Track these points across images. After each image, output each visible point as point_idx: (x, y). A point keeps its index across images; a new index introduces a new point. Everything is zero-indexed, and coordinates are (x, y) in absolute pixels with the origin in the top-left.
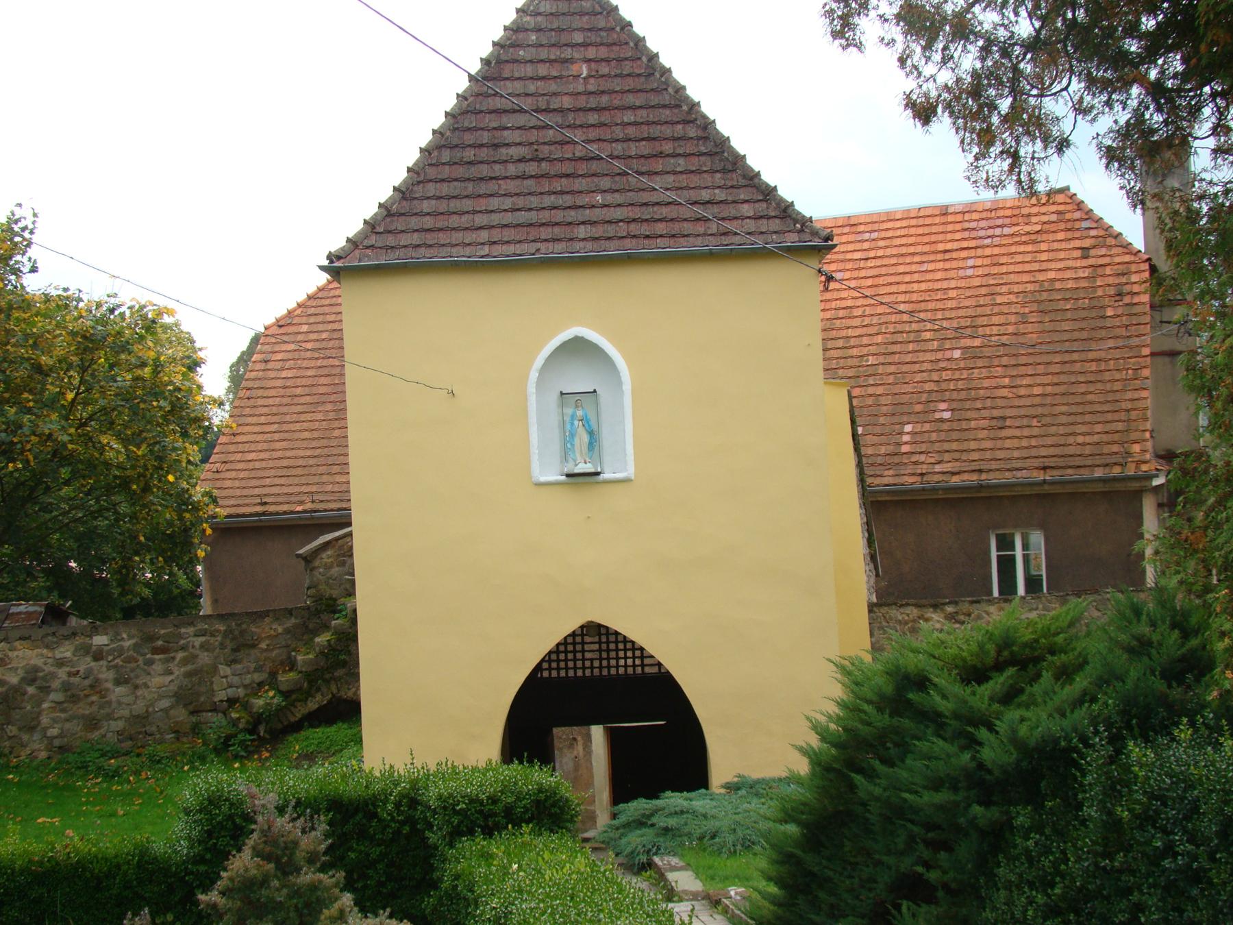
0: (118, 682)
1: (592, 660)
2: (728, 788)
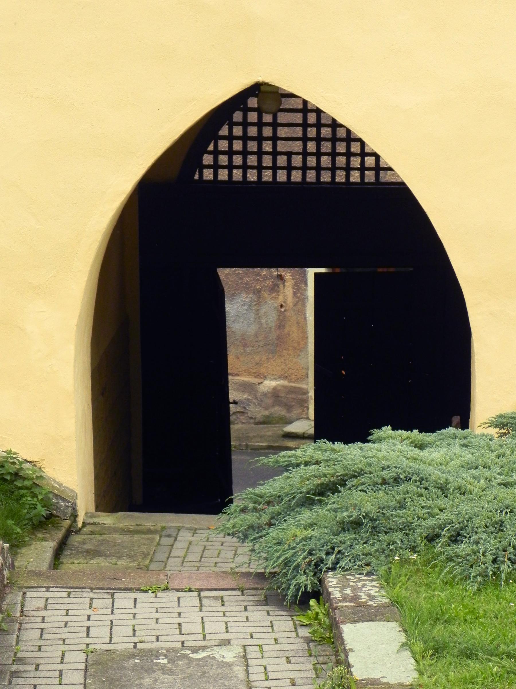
1: (289, 155)
2: (502, 426)
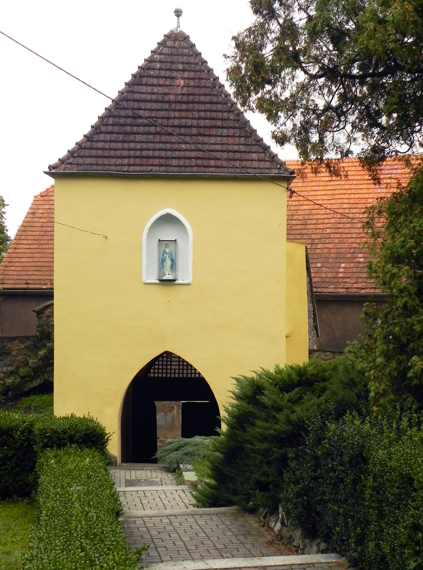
1: (175, 369)
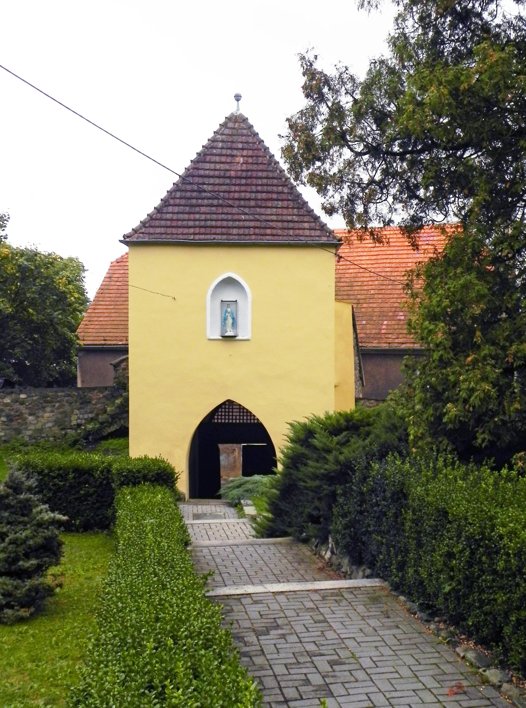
0: (30, 415)
1: (236, 416)
